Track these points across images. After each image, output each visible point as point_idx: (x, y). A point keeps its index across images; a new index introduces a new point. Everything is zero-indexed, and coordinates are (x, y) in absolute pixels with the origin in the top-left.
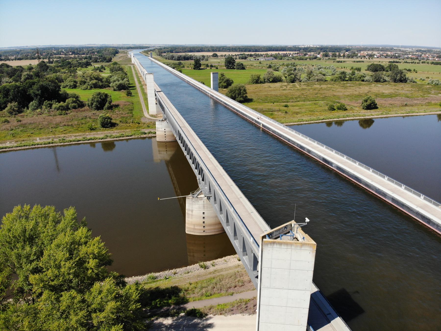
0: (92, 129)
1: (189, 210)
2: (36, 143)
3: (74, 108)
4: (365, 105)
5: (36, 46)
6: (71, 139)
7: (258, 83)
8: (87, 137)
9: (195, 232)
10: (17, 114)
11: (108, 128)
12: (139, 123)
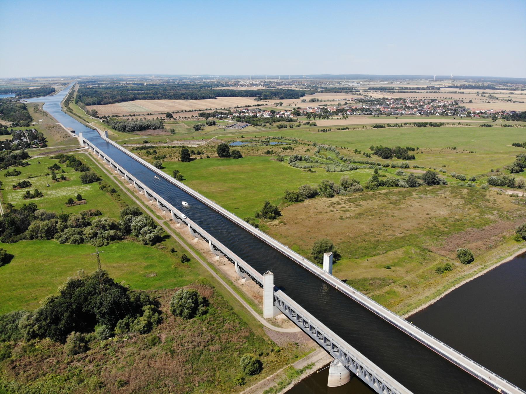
7: (298, 201)
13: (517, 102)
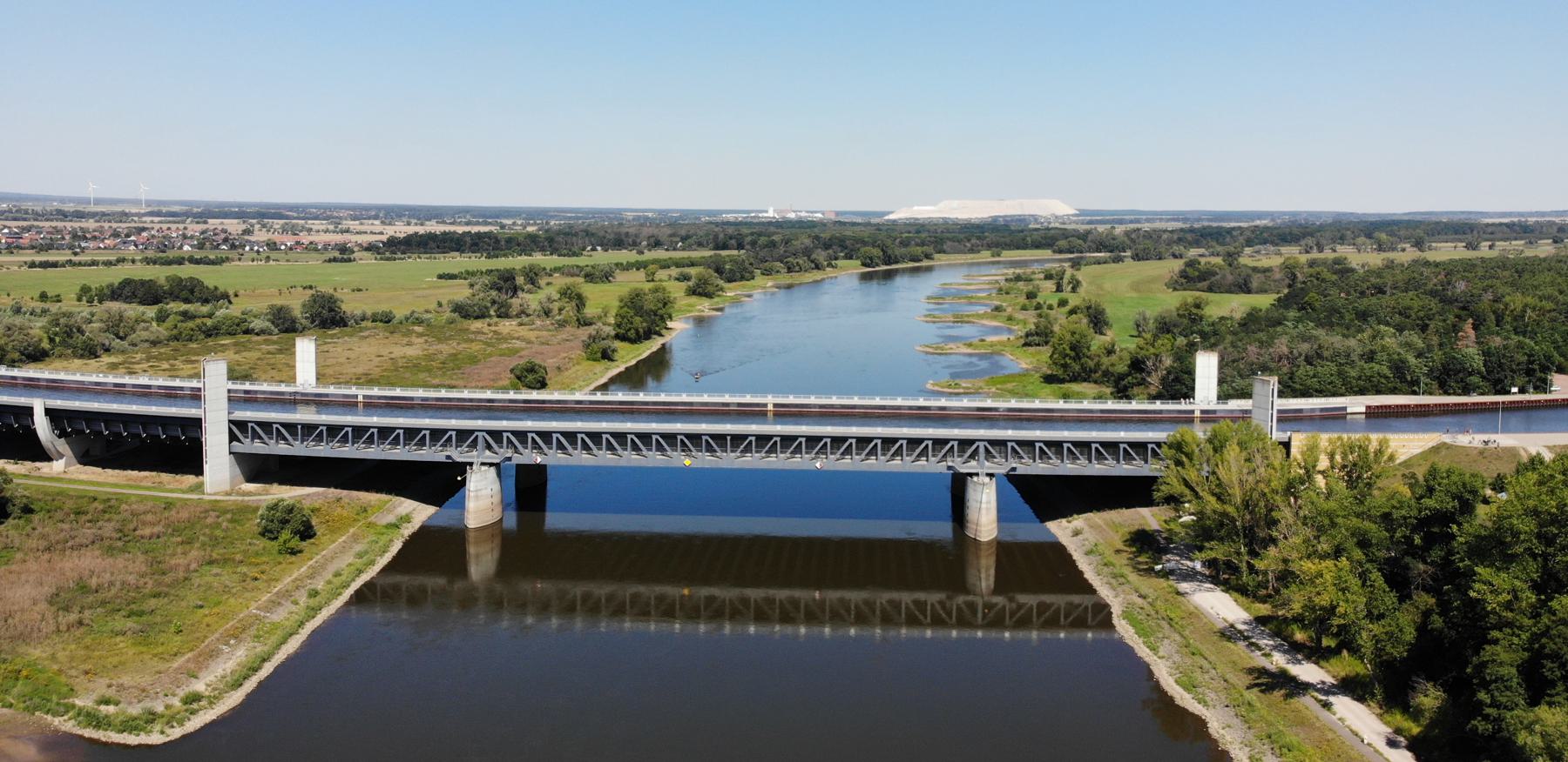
13: (366, 233)
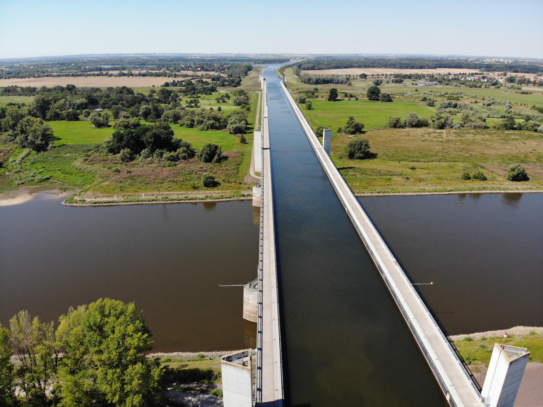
0: (195, 188)
1: (246, 298)
2: (141, 199)
3: (184, 158)
4: (511, 175)
5: (165, 54)
6: (173, 198)
7: (396, 127)
8: (189, 196)
9: (250, 319)
10: (129, 162)
11: (210, 187)
12: (241, 183)
